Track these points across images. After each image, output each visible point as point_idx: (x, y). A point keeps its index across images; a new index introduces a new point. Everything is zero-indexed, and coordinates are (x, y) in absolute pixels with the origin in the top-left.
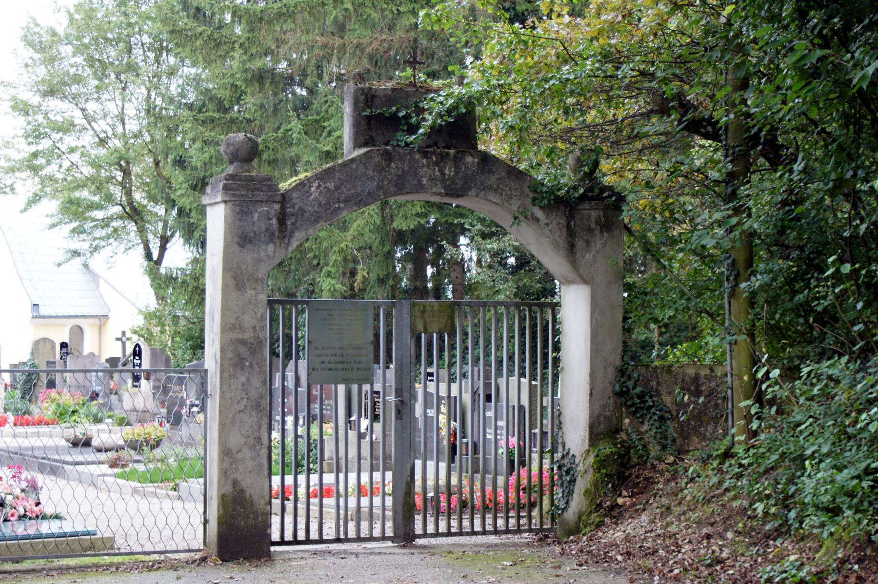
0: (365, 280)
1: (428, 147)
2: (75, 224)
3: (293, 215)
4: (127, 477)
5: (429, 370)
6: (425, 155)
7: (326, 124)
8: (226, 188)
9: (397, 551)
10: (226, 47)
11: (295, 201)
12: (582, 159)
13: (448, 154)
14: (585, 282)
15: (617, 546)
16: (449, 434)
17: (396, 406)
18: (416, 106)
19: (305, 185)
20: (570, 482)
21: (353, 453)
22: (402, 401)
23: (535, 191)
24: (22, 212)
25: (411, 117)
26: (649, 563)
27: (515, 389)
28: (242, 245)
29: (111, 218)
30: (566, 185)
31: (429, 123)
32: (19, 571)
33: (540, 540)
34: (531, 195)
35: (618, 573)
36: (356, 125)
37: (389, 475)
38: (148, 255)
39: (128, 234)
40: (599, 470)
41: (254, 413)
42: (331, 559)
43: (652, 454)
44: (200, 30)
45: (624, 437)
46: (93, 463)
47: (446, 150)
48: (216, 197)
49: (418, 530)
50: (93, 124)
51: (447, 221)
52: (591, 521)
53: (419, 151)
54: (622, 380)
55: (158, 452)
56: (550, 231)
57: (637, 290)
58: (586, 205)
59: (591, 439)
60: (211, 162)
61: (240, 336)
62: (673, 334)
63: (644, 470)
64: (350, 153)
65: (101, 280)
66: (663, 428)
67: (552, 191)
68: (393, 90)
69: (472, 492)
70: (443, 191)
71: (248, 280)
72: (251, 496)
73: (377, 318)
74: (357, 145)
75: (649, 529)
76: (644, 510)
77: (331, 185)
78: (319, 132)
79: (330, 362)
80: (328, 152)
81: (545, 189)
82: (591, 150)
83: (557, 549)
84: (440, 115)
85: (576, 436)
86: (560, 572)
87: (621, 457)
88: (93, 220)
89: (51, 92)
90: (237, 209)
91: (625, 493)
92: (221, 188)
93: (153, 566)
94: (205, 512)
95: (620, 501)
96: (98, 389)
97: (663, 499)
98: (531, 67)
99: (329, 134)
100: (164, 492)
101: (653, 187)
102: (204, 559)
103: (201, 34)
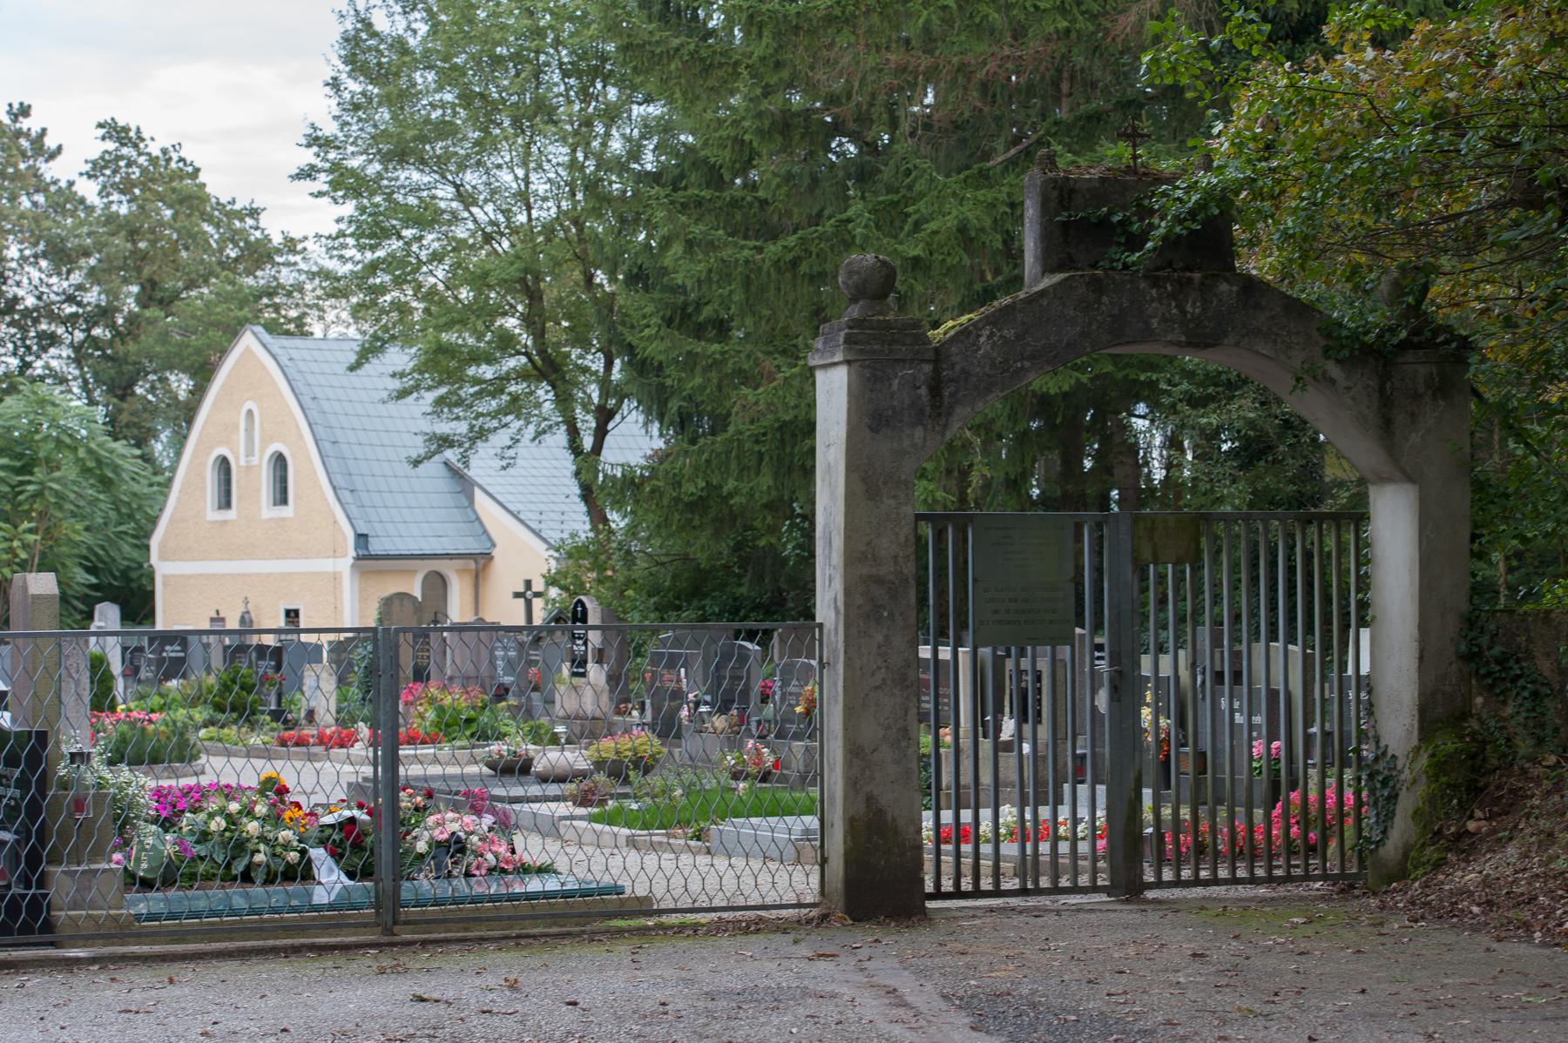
0: (987, 485)
1: (1157, 269)
2: (443, 390)
3: (952, 381)
4: (610, 819)
5: (1098, 640)
6: (1155, 282)
7: (910, 209)
8: (849, 340)
9: (1118, 907)
10: (721, 73)
11: (955, 359)
12: (1404, 283)
13: (1190, 280)
14: (1410, 479)
15: (1471, 894)
16: (1158, 741)
17: (1111, 680)
18: (1139, 205)
19: (970, 333)
20: (1388, 799)
21: (986, 778)
22: (1120, 673)
23: (1328, 336)
24: (352, 369)
25: (1131, 223)
26: (1526, 915)
27: (1280, 663)
28: (875, 429)
29: (505, 379)
30: (1377, 326)
31: (1162, 231)
32: (547, 935)
33: (1342, 891)
34: (1323, 342)
35: (1475, 929)
36: (1046, 238)
37: (1101, 790)
38: (575, 447)
39: (538, 405)
40: (1436, 777)
41: (896, 691)
42: (1018, 920)
43: (1522, 752)
44: (676, 42)
45: (1476, 726)
46: (536, 799)
47: (1188, 274)
48: (833, 355)
49: (1149, 877)
50: (475, 210)
51: (1126, 377)
52: (1425, 859)
53: (1146, 277)
54: (1471, 635)
55: (655, 780)
56: (1353, 399)
57: (1492, 491)
58: (1410, 356)
59: (1421, 729)
60: (709, 279)
61: (874, 571)
62: (1531, 569)
63: (1509, 777)
64: (1036, 281)
65: (477, 491)
66: (1539, 710)
67: (1355, 336)
68: (1103, 180)
69: (1214, 831)
70: (1183, 339)
71: (885, 483)
72: (894, 819)
73: (1078, 538)
74: (1048, 269)
75: (1519, 866)
76: (1511, 839)
77: (1009, 333)
78: (897, 223)
79: (1008, 611)
80: (916, 259)
81: (1345, 333)
82: (1416, 268)
83: (1374, 902)
84: (1178, 220)
85: (1397, 725)
86: (1384, 931)
87: (1473, 757)
88: (477, 381)
89: (400, 154)
90: (867, 373)
91: (1478, 814)
92: (841, 340)
93: (748, 927)
94: (822, 846)
95: (1471, 826)
96: (508, 679)
97: (1542, 822)
98: (1320, 140)
99: (917, 226)
100: (682, 842)
101: (1517, 326)
102: (824, 917)
103: (677, 50)
